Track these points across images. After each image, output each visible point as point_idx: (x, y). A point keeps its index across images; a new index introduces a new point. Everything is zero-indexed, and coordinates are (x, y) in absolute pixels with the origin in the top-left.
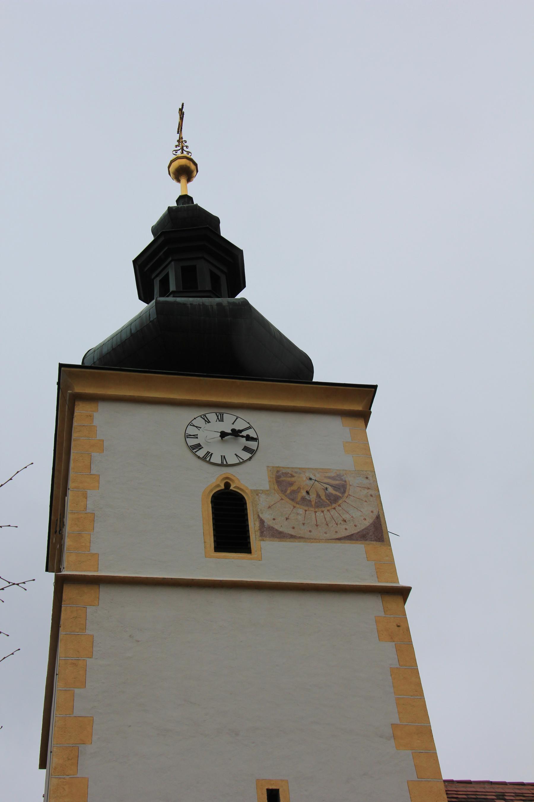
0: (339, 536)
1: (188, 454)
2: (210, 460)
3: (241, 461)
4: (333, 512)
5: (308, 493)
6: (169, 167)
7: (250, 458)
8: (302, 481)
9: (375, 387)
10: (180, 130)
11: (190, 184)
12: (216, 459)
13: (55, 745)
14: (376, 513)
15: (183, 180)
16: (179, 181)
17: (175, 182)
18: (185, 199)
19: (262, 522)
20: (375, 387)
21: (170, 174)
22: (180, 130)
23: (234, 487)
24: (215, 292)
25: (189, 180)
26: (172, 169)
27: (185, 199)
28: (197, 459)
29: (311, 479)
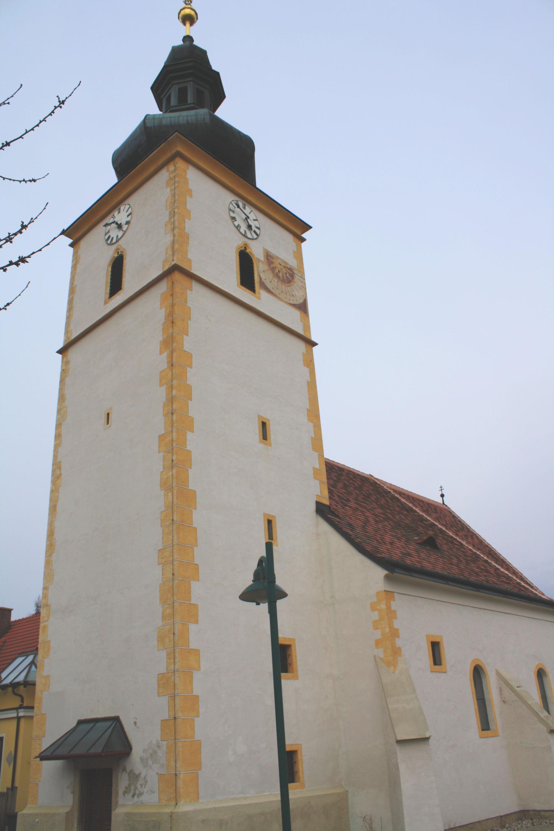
0: (289, 302)
1: (230, 221)
2: (234, 221)
3: (253, 238)
4: (288, 288)
5: (279, 271)
6: (181, 10)
7: (256, 239)
8: (276, 263)
9: (310, 227)
10: (28, 285)
11: (192, 27)
12: (236, 223)
13: (177, 522)
14: (304, 298)
15: (188, 24)
16: (185, 24)
17: (181, 25)
18: (188, 39)
19: (260, 278)
20: (310, 227)
21: (179, 18)
22: (28, 285)
23: (249, 252)
24: (199, 104)
25: (192, 24)
26: (183, 13)
27: (188, 39)
28: (233, 225)
29: (280, 264)
